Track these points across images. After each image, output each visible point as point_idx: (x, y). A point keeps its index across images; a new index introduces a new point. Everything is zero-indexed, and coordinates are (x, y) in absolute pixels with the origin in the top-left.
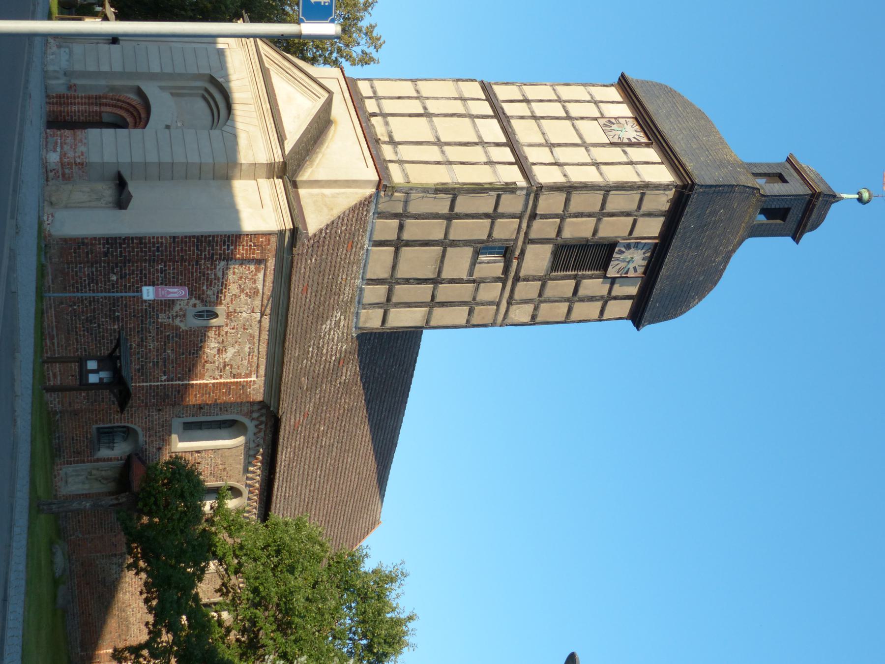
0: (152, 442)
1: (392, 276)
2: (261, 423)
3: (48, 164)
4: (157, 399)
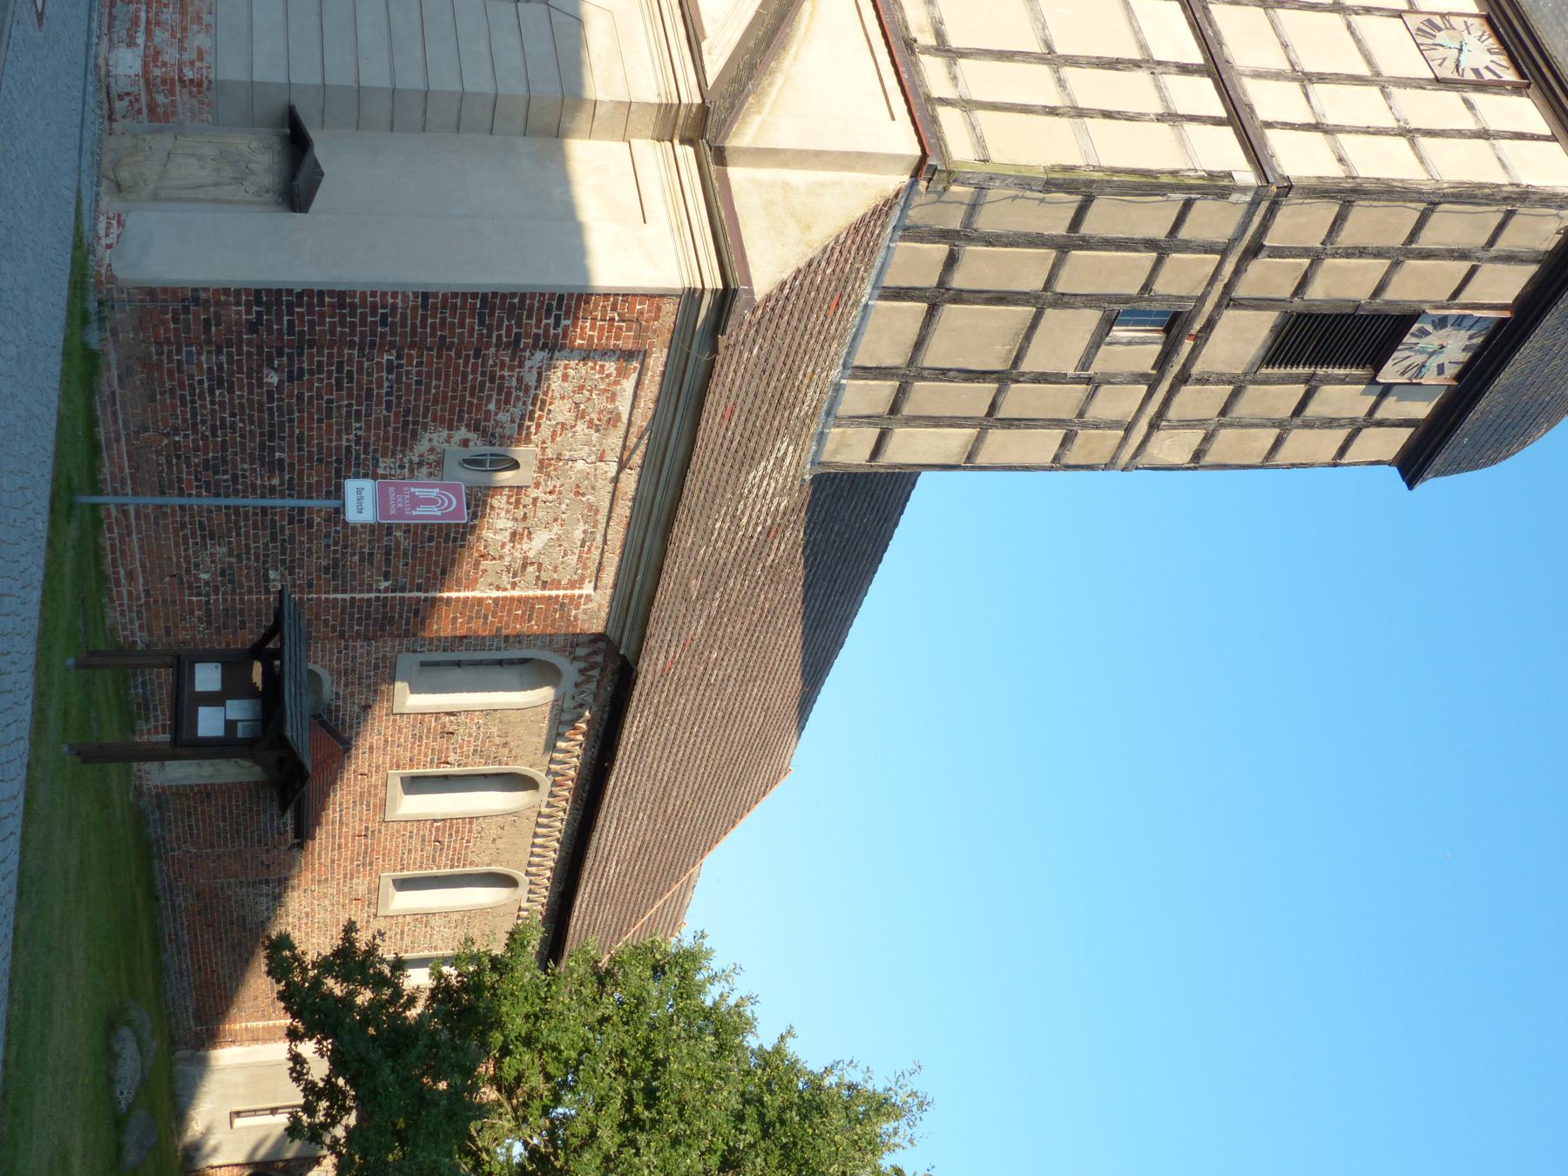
0: (352, 694)
1: (912, 361)
2: (592, 667)
3: (112, 80)
4: (367, 626)
